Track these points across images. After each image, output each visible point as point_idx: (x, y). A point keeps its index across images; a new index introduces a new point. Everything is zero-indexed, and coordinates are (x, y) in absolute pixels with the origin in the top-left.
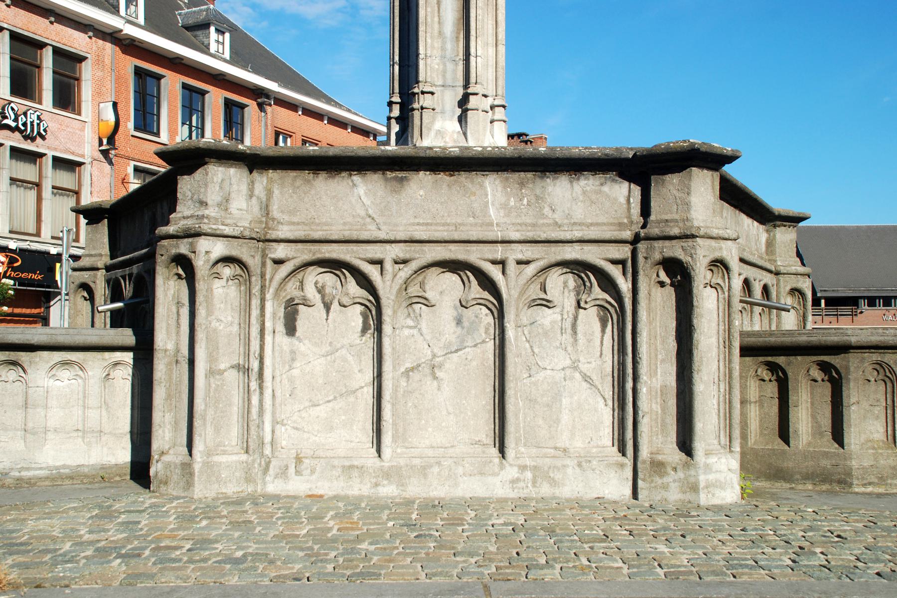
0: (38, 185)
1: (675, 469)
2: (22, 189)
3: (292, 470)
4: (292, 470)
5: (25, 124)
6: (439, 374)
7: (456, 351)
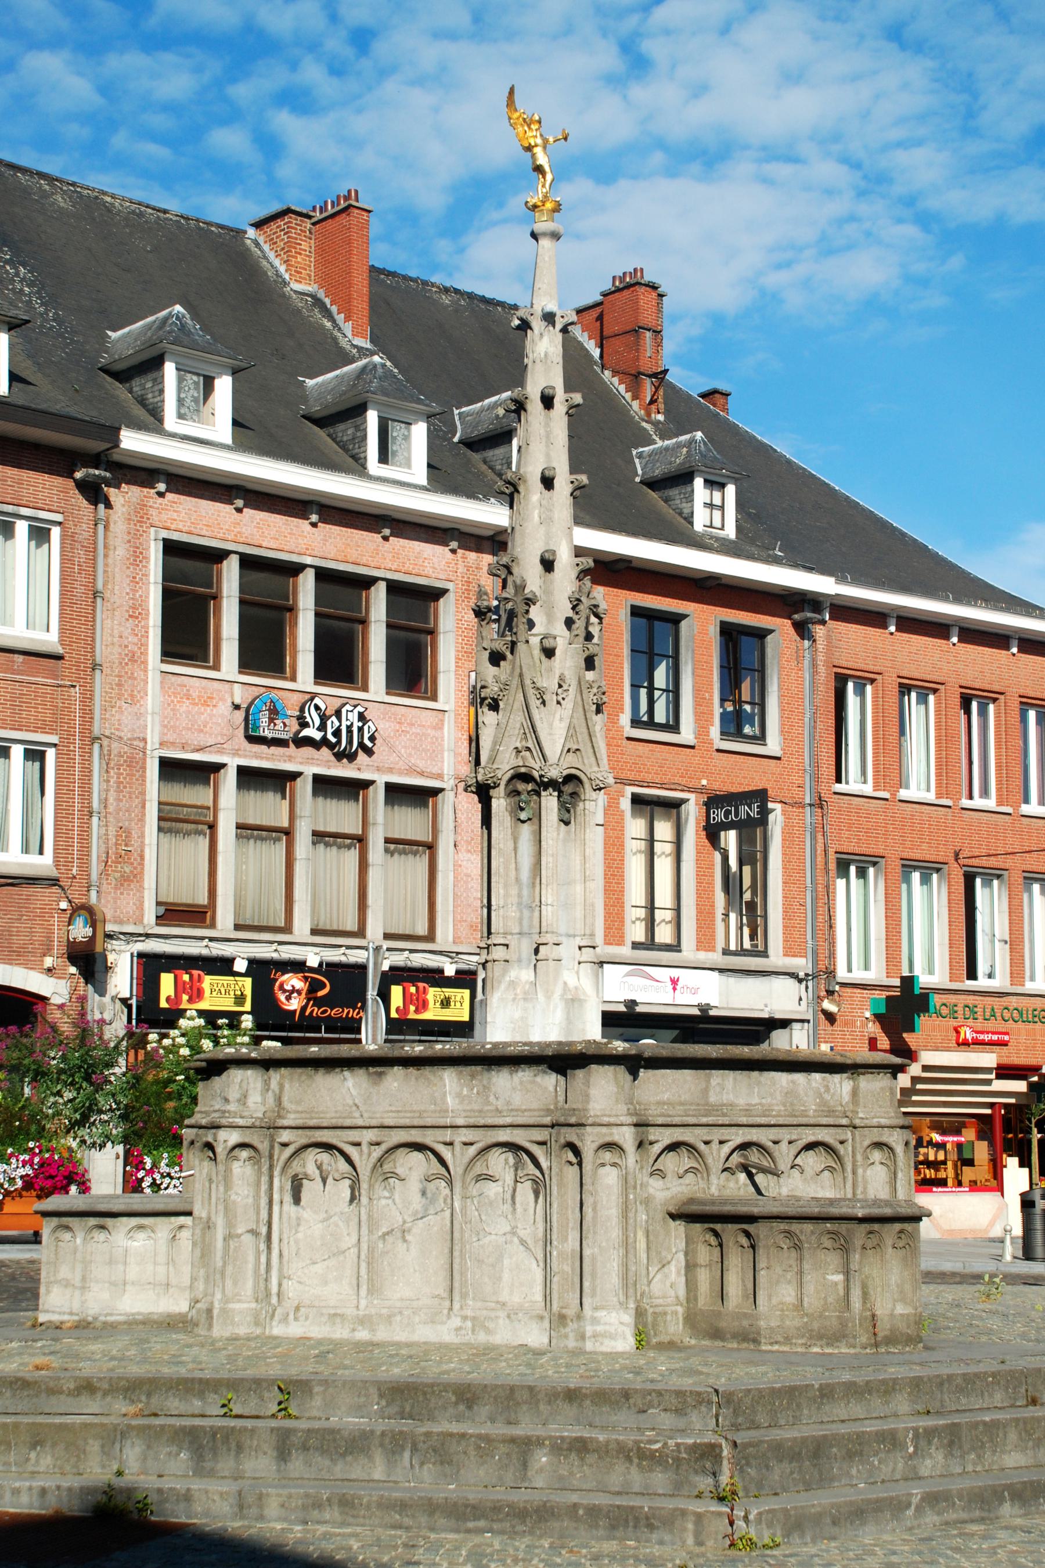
0: (360, 840)
1: (572, 1320)
2: (334, 849)
3: (291, 1316)
4: (291, 1316)
5: (337, 733)
6: (408, 1237)
7: (422, 1218)
